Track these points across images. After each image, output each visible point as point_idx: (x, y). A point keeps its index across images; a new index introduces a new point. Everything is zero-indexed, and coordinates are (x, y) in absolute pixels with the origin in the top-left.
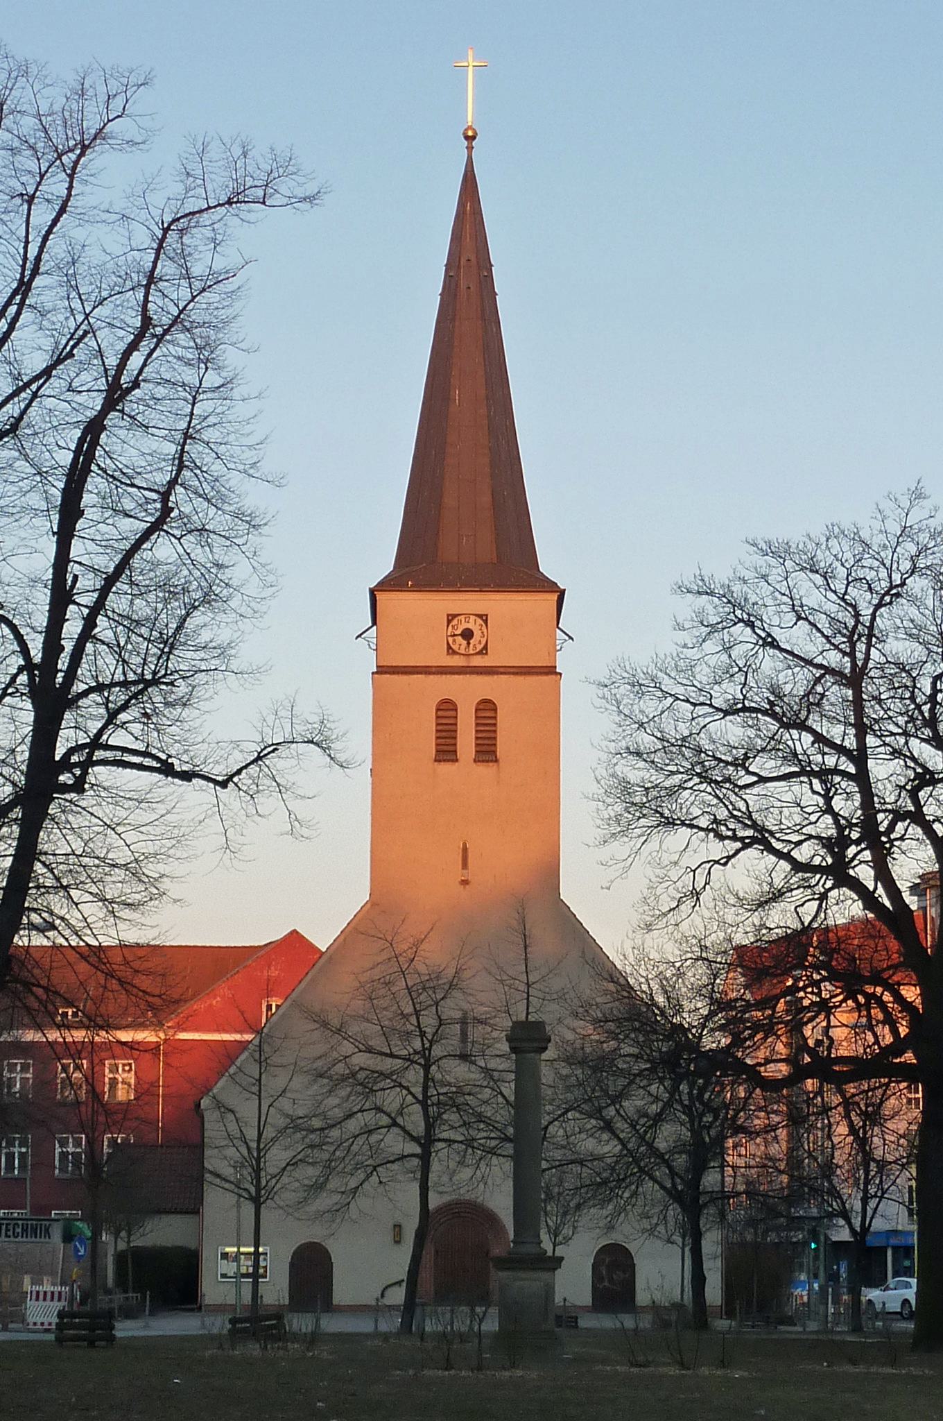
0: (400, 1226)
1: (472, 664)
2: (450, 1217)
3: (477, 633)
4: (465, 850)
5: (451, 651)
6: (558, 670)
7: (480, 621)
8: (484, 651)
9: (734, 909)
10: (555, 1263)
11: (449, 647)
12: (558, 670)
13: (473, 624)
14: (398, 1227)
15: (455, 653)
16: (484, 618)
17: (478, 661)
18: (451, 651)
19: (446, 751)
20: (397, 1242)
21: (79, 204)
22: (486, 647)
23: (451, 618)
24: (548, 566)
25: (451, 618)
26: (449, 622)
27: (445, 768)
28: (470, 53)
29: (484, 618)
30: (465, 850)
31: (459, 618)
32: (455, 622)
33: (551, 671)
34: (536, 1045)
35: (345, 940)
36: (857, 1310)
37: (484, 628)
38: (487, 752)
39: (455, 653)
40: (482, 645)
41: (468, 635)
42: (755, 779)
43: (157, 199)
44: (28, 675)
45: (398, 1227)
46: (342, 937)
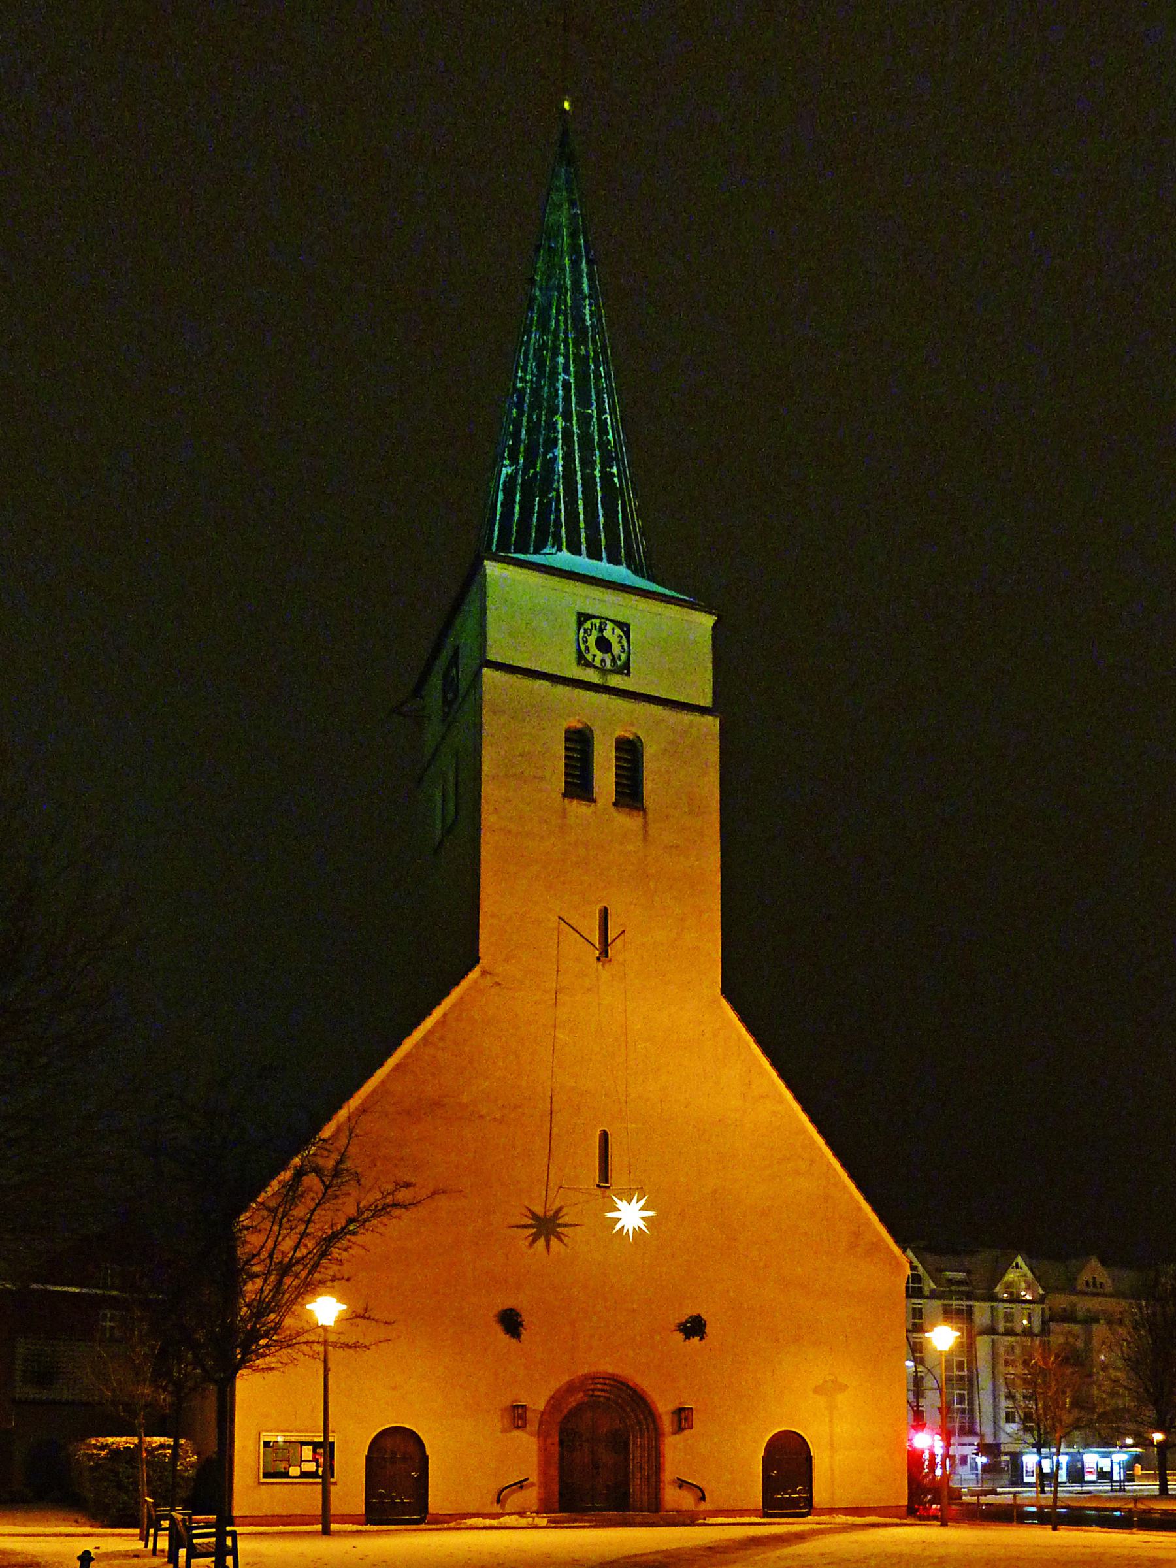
17: (615, 681)
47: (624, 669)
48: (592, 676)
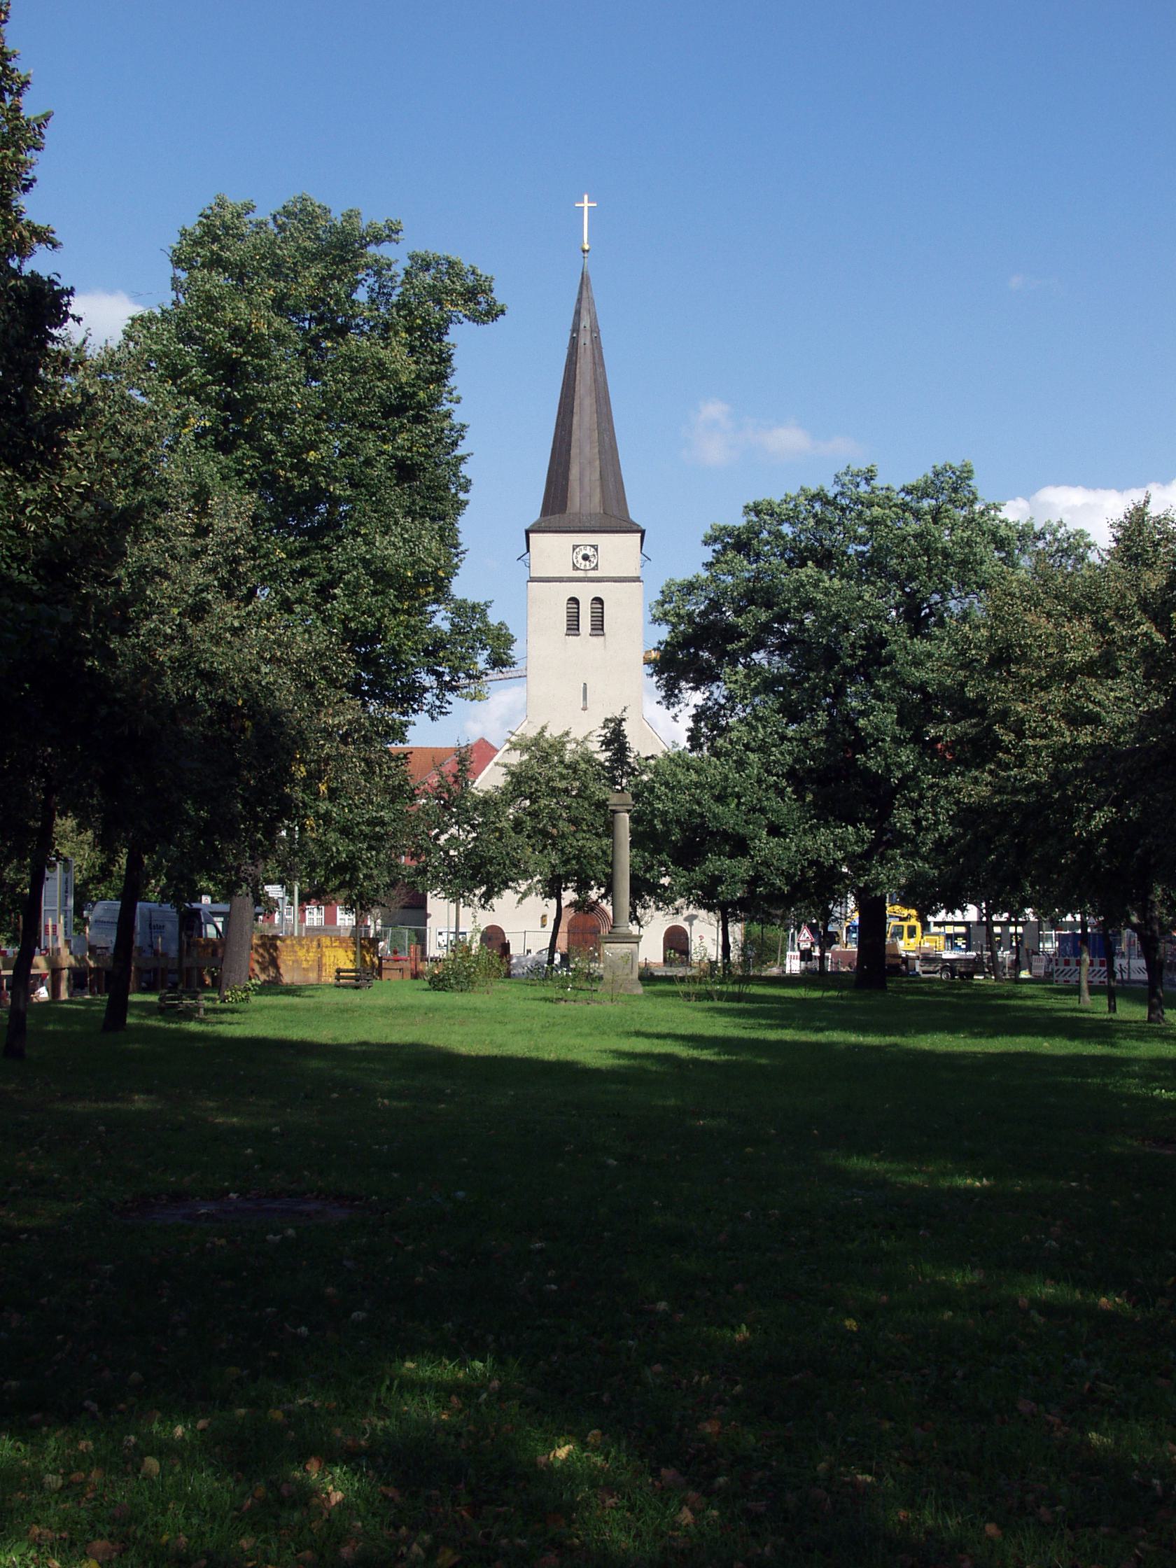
4: (584, 282)
5: (575, 568)
7: (578, 565)
8: (575, 547)
10: (636, 940)
11: (596, 550)
13: (590, 552)
14: (544, 917)
15: (578, 569)
16: (595, 547)
17: (592, 574)
18: (575, 568)
19: (573, 627)
22: (597, 565)
23: (575, 547)
24: (635, 515)
26: (574, 550)
28: (586, 197)
29: (595, 547)
30: (584, 282)
32: (578, 550)
34: (626, 808)
38: (598, 627)
39: (578, 569)
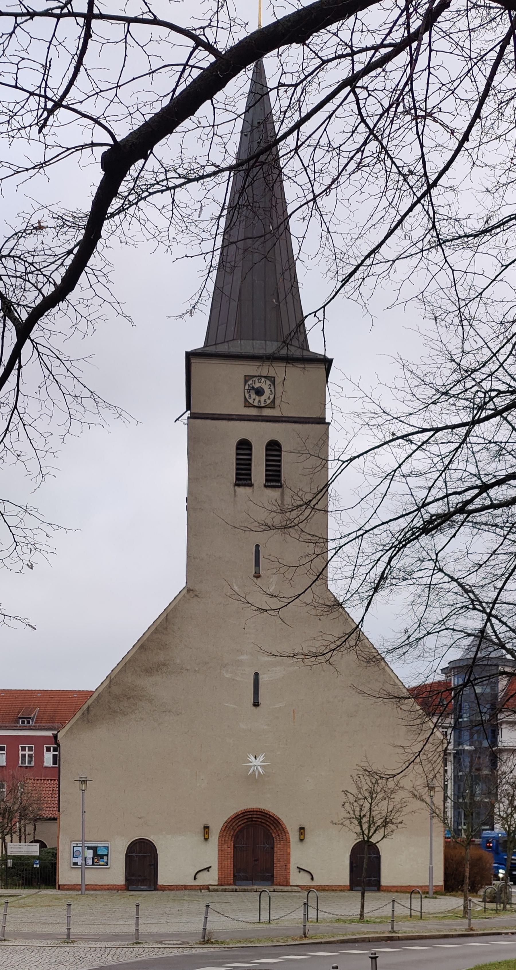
0: (208, 828)
1: (262, 415)
2: (246, 821)
3: (267, 392)
5: (248, 405)
6: (327, 421)
7: (268, 382)
9: (455, 596)
12: (327, 421)
14: (206, 828)
16: (272, 380)
17: (267, 412)
18: (248, 405)
20: (206, 839)
21: (426, 465)
25: (247, 378)
26: (246, 382)
27: (241, 490)
31: (254, 379)
33: (321, 421)
35: (167, 616)
36: (490, 799)
37: (272, 387)
40: (271, 400)
41: (259, 392)
42: (66, 149)
43: (417, 653)
44: (220, 53)
45: (206, 828)
46: (165, 614)
47: (272, 406)
48: (253, 412)
